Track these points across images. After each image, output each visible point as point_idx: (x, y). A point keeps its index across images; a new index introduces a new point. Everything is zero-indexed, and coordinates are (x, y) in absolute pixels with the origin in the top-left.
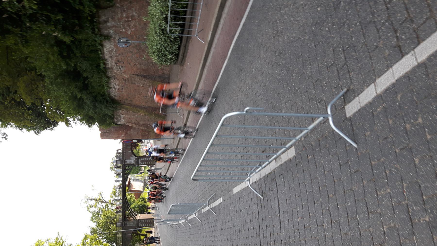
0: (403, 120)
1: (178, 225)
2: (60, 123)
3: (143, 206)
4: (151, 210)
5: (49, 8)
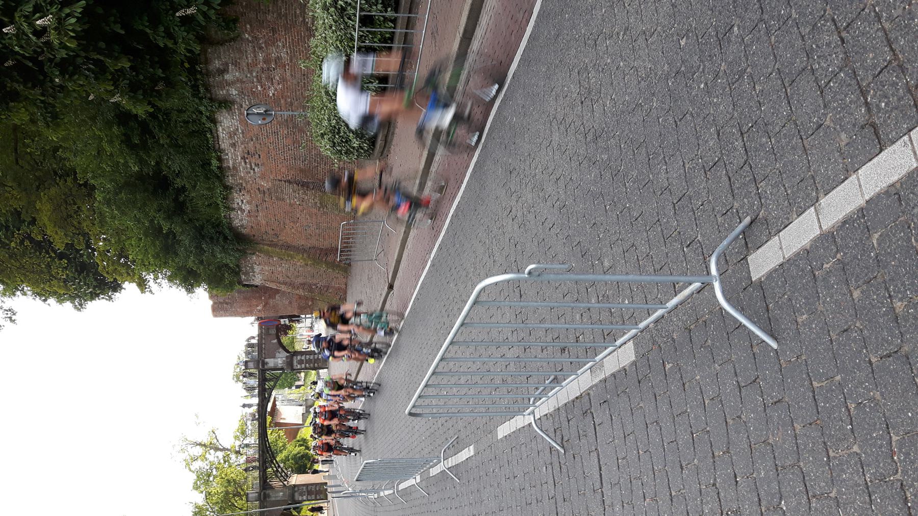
0: (887, 289)
1: (378, 500)
2: (126, 285)
3: (303, 456)
4: (321, 465)
5: (102, 45)
